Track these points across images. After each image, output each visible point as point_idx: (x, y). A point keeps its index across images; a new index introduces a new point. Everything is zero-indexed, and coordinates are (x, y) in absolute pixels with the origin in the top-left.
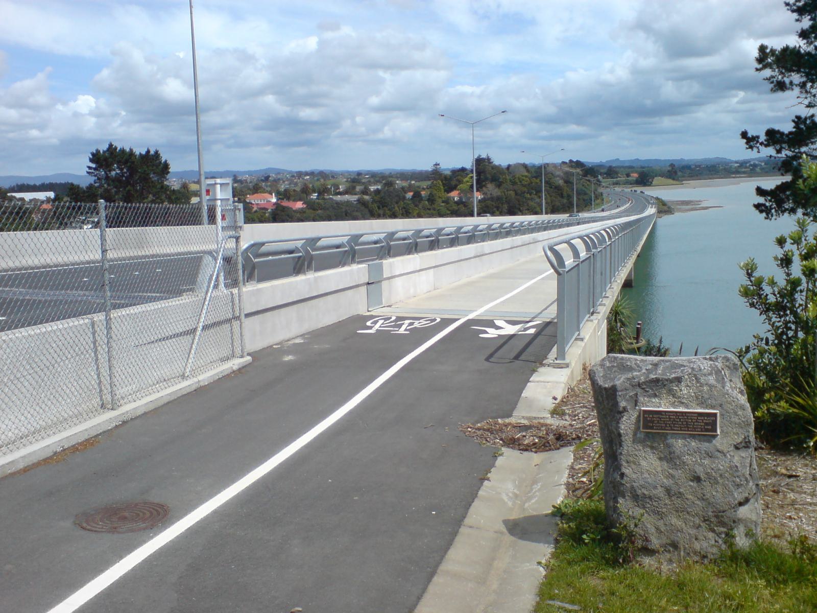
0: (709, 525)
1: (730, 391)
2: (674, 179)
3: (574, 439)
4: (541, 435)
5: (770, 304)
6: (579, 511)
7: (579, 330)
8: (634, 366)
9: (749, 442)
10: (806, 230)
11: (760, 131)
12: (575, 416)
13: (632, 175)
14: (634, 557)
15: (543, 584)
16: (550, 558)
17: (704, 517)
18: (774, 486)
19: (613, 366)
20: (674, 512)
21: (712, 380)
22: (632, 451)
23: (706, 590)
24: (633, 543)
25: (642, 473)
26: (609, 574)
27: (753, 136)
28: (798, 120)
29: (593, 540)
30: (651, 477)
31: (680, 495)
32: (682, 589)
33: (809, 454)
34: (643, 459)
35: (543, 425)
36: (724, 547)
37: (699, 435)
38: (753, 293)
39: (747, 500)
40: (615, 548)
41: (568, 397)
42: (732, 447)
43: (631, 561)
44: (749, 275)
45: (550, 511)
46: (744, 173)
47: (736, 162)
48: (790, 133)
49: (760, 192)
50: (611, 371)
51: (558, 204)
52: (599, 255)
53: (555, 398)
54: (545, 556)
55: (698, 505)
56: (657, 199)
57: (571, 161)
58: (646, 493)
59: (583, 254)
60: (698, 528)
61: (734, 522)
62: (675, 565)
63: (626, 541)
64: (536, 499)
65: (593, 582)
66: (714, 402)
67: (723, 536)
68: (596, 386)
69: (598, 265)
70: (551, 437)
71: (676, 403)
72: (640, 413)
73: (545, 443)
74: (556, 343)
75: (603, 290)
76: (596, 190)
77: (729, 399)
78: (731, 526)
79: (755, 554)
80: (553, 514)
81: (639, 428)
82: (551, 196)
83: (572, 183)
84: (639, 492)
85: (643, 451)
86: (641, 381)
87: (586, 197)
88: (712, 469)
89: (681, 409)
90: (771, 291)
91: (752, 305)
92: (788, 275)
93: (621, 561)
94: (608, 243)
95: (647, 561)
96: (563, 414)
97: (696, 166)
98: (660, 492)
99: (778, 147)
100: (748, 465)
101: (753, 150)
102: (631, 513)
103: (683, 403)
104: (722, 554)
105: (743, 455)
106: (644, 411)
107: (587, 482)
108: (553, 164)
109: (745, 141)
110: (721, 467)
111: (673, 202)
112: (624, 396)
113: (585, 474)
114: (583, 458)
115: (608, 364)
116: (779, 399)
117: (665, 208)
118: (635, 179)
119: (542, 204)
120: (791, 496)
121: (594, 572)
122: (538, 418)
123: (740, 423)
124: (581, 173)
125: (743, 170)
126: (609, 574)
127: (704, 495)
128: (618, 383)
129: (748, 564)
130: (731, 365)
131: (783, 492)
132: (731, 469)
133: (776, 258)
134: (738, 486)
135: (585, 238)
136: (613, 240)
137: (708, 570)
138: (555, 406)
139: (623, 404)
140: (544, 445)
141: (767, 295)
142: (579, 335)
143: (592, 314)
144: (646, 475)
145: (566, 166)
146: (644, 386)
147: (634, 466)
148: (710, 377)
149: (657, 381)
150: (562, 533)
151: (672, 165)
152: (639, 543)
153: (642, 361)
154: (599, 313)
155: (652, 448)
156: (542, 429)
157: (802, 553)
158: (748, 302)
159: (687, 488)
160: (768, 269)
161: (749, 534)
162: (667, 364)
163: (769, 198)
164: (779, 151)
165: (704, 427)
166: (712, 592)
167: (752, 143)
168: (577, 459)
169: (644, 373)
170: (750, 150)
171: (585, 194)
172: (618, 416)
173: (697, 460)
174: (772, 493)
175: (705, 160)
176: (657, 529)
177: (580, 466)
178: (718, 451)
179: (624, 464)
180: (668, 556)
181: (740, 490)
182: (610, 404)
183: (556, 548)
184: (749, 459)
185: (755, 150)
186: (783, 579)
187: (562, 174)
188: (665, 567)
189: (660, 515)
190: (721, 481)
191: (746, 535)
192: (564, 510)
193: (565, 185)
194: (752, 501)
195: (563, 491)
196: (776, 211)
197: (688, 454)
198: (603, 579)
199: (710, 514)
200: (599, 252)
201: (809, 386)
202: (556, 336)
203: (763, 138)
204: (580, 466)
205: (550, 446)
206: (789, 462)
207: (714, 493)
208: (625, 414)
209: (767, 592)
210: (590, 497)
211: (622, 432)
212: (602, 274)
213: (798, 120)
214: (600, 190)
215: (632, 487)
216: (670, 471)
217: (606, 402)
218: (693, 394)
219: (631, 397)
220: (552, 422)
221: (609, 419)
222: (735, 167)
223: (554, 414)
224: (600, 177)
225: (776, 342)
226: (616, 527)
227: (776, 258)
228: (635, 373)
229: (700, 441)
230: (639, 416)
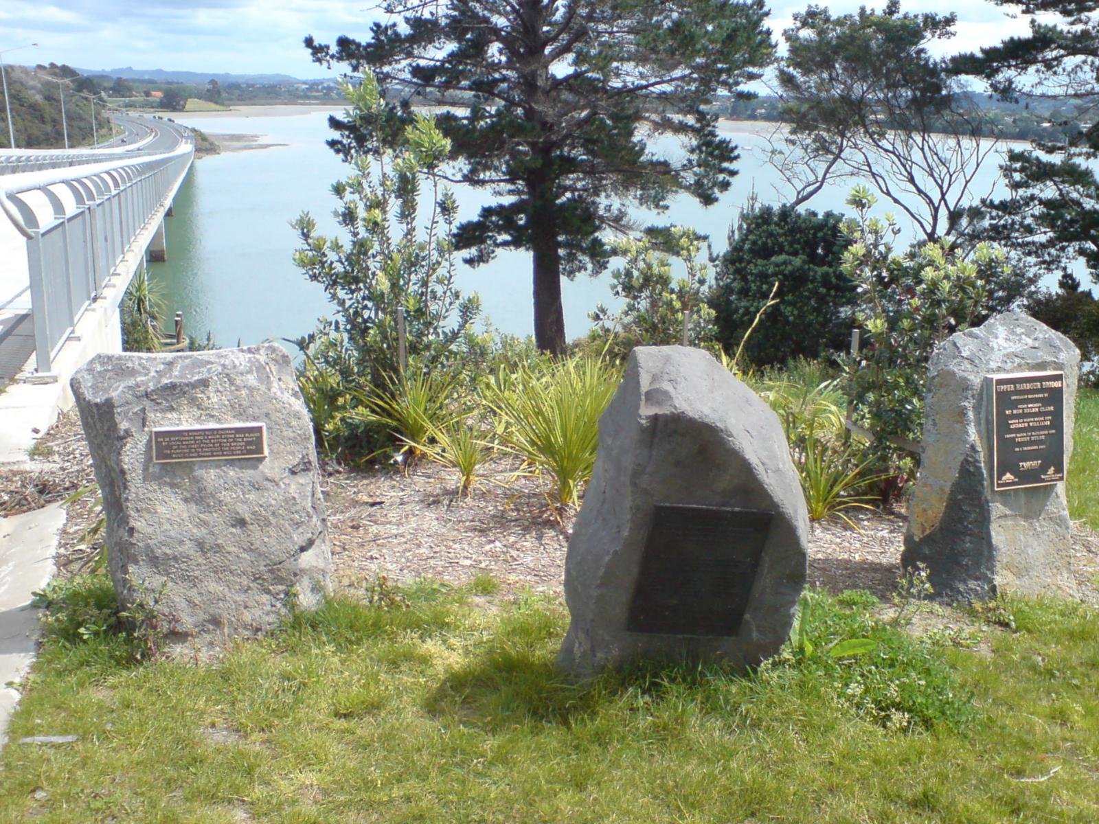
0: (262, 585)
1: (279, 393)
2: (216, 103)
3: (67, 489)
4: (12, 488)
5: (337, 275)
6: (75, 595)
7: (72, 324)
8: (137, 367)
9: (310, 462)
10: (369, 173)
11: (329, 40)
12: (69, 454)
13: (153, 93)
14: (158, 647)
15: (16, 715)
16: (28, 673)
17: (254, 575)
18: (353, 520)
19: (107, 371)
20: (212, 574)
21: (252, 380)
22: (144, 494)
23: (260, 675)
24: (155, 628)
25: (160, 524)
26: (122, 679)
27: (320, 45)
28: (378, 29)
29: (96, 634)
30: (174, 529)
31: (218, 548)
32: (226, 680)
33: (397, 472)
34: (161, 504)
35: (15, 473)
36: (283, 611)
37: (239, 459)
38: (314, 263)
39: (311, 543)
40: (129, 640)
41: (57, 427)
42: (288, 473)
43: (153, 655)
44: (306, 236)
45: (28, 602)
46: (316, 98)
47: (304, 83)
48: (369, 45)
49: (335, 124)
50: (104, 378)
51: (35, 132)
52: (99, 211)
53: (36, 431)
54: (17, 670)
55: (245, 559)
56: (194, 130)
57: (53, 65)
58: (168, 551)
59: (71, 208)
60: (246, 591)
61: (295, 575)
62: (218, 649)
63: (144, 627)
64: (6, 586)
65: (98, 695)
66: (256, 410)
67: (282, 596)
68: (82, 402)
69: (99, 224)
70: (30, 489)
71: (203, 418)
72: (151, 437)
73: (20, 500)
74: (35, 349)
75: (110, 262)
76: (99, 114)
77: (278, 406)
78: (291, 581)
79: (323, 613)
80: (34, 606)
81: (152, 458)
82: (23, 120)
83: (59, 101)
84: (158, 552)
85: (159, 492)
86: (149, 390)
87: (82, 124)
88: (261, 506)
89: (212, 425)
90: (337, 258)
91: (314, 277)
92: (355, 234)
93: (138, 657)
94: (114, 192)
95: (178, 650)
96: (50, 453)
97: (249, 86)
98: (189, 548)
99: (354, 62)
100: (309, 494)
101: (321, 64)
102: (146, 584)
103: (212, 416)
104: (281, 621)
105: (302, 481)
106: (156, 433)
107: (88, 550)
108: (20, 67)
109: (310, 51)
110: (273, 502)
111: (218, 136)
112: (126, 413)
113: (82, 539)
114: (80, 516)
115: (99, 368)
116: (357, 402)
117: (206, 145)
118: (158, 100)
119: (8, 132)
120: (374, 529)
121: (98, 681)
122: (9, 463)
123: (295, 438)
124: (72, 85)
125: (315, 94)
126: (122, 679)
127: (252, 544)
128: (114, 394)
129: (314, 627)
130: (279, 358)
131: (364, 525)
132: (287, 503)
133: (336, 213)
134: (298, 525)
135: (75, 183)
136: (122, 188)
137: (262, 647)
138: (36, 444)
139: (124, 425)
140: (18, 504)
141: (332, 263)
142: (73, 332)
143: (95, 299)
144: (166, 526)
145: (44, 72)
146: (155, 397)
147: (147, 516)
148: (249, 376)
149: (173, 386)
150: (47, 631)
151: (213, 82)
152: (164, 627)
153: (148, 359)
154: (105, 298)
155: (172, 485)
156: (14, 479)
157: (381, 599)
158: (307, 273)
159: (228, 537)
160: (330, 230)
161: (317, 588)
162: (187, 361)
163: (347, 133)
164: (355, 69)
165: (243, 447)
166: (268, 676)
167: (319, 55)
168: (73, 517)
169: (154, 377)
170: (318, 63)
171: (82, 119)
172: (118, 444)
173: (239, 496)
174: (350, 530)
175: (262, 77)
176: (189, 601)
177: (77, 528)
178: (268, 479)
179: (133, 513)
180: (208, 637)
181: (301, 530)
182: (106, 428)
183: (38, 656)
184: (311, 485)
185: (325, 64)
186: (357, 638)
187: (39, 85)
188: (203, 656)
189: (192, 581)
190: (273, 521)
191: (313, 590)
192: (51, 596)
193: (46, 102)
194: (317, 542)
195: (50, 568)
196: (356, 151)
197: (226, 489)
198: (113, 687)
199: (262, 568)
200: (98, 205)
201: (393, 383)
202: (33, 336)
203: (334, 49)
204: (77, 528)
205: (29, 504)
206: (372, 486)
207: (266, 539)
208: (129, 439)
209: (336, 659)
210: (93, 571)
211: (125, 467)
212: (106, 239)
213: (378, 29)
214: (105, 114)
215: (148, 546)
216: (202, 516)
217: (98, 426)
218: (226, 403)
219: (135, 414)
220: (33, 467)
221: (105, 449)
222: (303, 90)
223: (34, 454)
224: (103, 94)
225: (349, 327)
226: (125, 609)
227: (336, 213)
228: (139, 379)
229: (241, 468)
230: (150, 441)
